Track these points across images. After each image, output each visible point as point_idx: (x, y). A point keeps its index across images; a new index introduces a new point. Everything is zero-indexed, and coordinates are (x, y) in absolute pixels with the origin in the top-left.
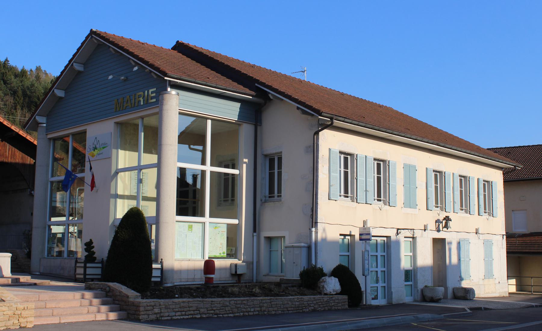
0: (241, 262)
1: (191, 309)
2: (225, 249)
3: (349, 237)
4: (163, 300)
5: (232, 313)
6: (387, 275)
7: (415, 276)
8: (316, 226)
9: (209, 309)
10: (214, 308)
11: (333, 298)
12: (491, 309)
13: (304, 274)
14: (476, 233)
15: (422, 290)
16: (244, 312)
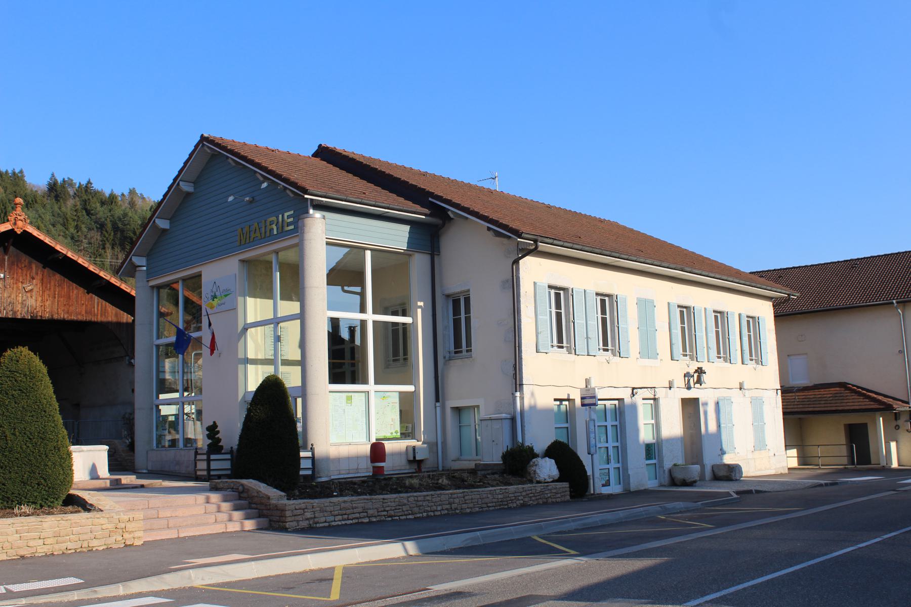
1: (355, 511)
2: (397, 427)
3: (567, 403)
6: (622, 452)
8: (521, 390)
10: (387, 509)
13: (506, 456)
16: (428, 511)
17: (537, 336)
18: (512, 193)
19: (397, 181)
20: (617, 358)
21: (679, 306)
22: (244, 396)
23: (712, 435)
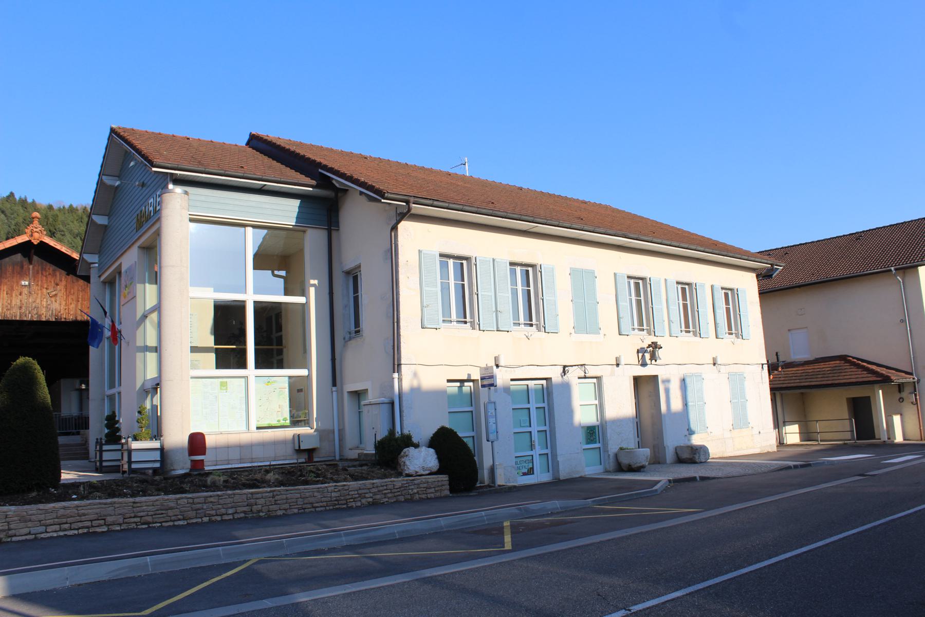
1: (83, 518)
2: (287, 415)
3: (471, 384)
4: (13, 508)
5: (184, 519)
6: (549, 436)
7: (604, 434)
8: (399, 371)
9: (128, 515)
10: (140, 514)
11: (416, 482)
13: (381, 446)
14: (714, 364)
16: (210, 516)
18: (490, 179)
22: (143, 385)
23: (675, 414)
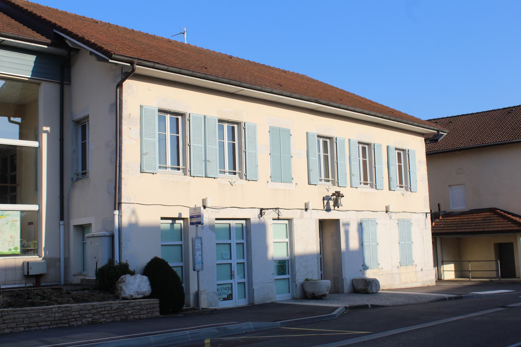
0: (41, 258)
2: (18, 244)
6: (247, 267)
8: (119, 209)
11: (131, 304)
12: (383, 306)
13: (100, 272)
14: (387, 212)
15: (302, 285)
17: (141, 157)
19: (39, 19)
20: (409, 192)
21: (396, 149)
23: (354, 252)
